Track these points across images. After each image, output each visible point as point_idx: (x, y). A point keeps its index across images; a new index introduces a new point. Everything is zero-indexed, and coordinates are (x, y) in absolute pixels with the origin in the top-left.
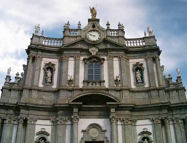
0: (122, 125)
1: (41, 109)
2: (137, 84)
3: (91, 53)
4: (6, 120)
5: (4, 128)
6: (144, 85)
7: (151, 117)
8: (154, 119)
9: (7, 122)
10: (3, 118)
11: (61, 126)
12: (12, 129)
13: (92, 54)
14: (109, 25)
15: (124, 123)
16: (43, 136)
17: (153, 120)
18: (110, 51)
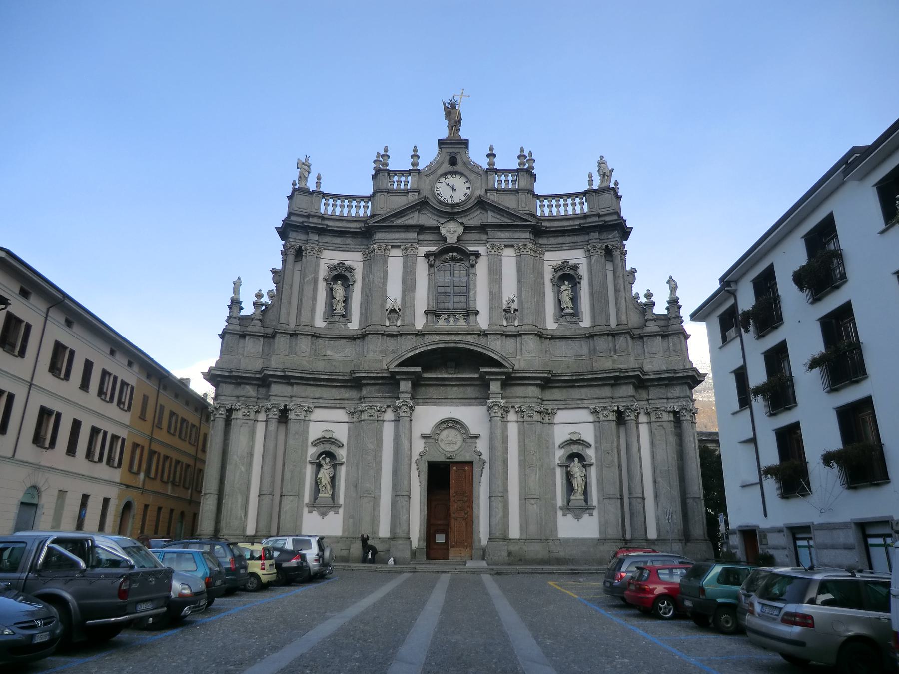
9: (240, 416)
12: (253, 432)
13: (449, 241)
17: (595, 412)
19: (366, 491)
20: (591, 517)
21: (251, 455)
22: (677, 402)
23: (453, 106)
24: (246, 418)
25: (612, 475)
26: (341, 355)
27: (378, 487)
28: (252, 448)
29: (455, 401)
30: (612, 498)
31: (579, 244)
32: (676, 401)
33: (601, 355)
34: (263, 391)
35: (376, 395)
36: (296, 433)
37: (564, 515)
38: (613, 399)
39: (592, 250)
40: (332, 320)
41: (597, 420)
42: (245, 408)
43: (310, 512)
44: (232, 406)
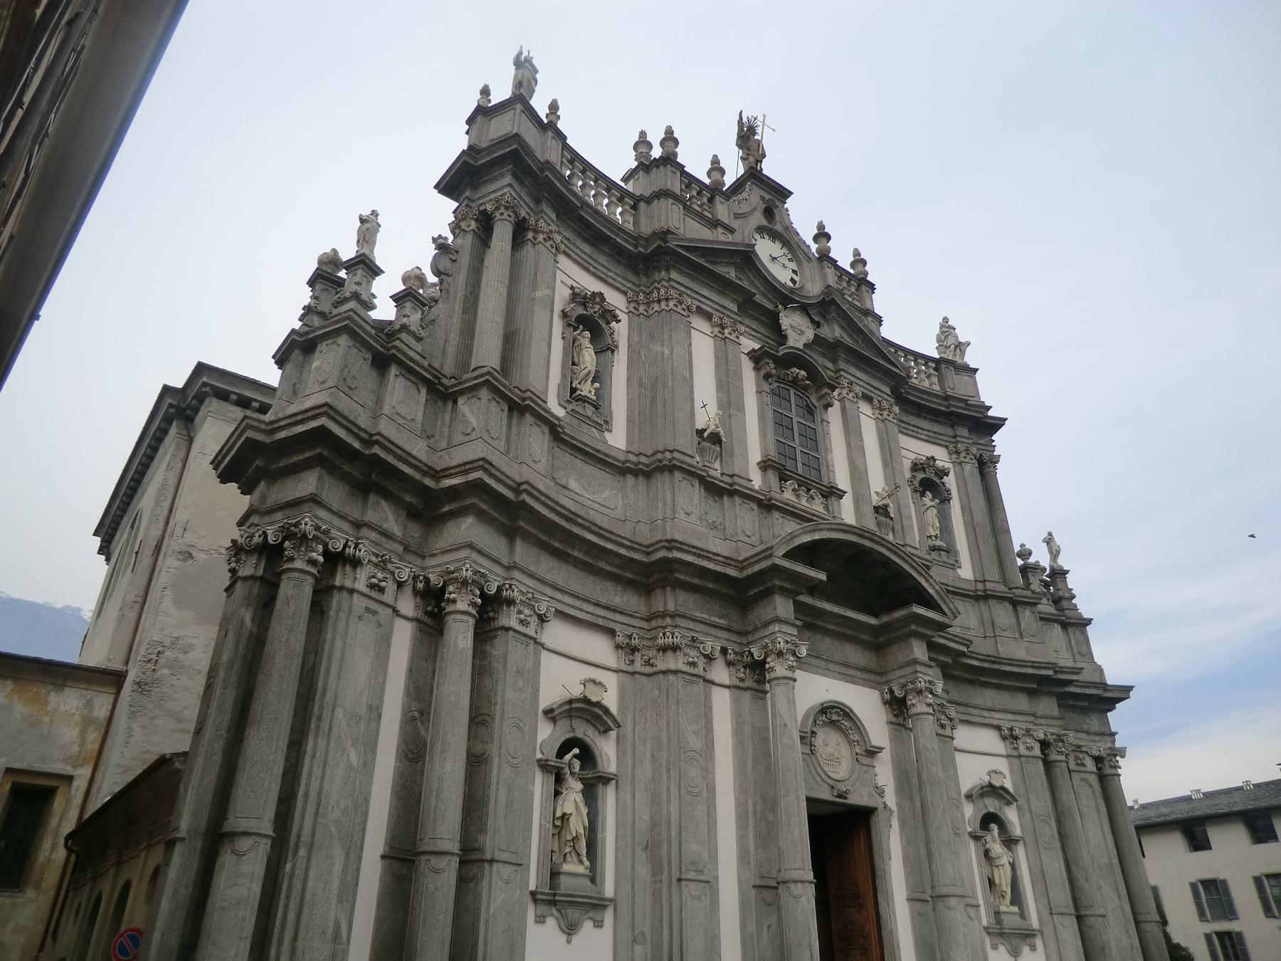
0: (1008, 756)
1: (602, 565)
2: (574, 406)
3: (785, 337)
4: (356, 563)
5: (341, 626)
6: (605, 426)
7: (1005, 721)
8: (1017, 732)
9: (361, 585)
10: (339, 546)
11: (691, 682)
12: (384, 642)
13: (791, 343)
14: (828, 237)
15: (632, 662)
16: (992, 805)
17: (1010, 737)
18: (848, 362)
19: (693, 863)
20: (598, 930)
21: (375, 712)
22: (1100, 741)
23: (752, 130)
24: (374, 594)
25: (1057, 864)
26: (596, 498)
27: (714, 856)
28: (379, 690)
29: (833, 667)
30: (1066, 914)
31: (941, 437)
32: (1097, 738)
33: (1003, 634)
34: (415, 531)
35: (698, 614)
36: (518, 671)
37: (995, 947)
38: (1035, 717)
39: (963, 454)
40: (579, 409)
41: (1015, 753)
42: (376, 565)
43: (540, 920)
44: (345, 546)
